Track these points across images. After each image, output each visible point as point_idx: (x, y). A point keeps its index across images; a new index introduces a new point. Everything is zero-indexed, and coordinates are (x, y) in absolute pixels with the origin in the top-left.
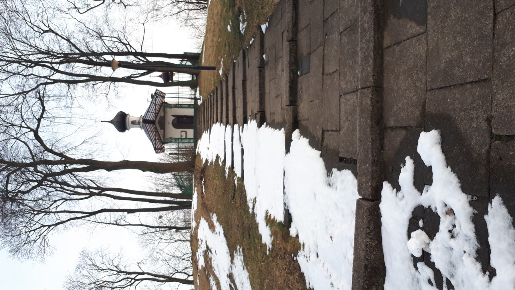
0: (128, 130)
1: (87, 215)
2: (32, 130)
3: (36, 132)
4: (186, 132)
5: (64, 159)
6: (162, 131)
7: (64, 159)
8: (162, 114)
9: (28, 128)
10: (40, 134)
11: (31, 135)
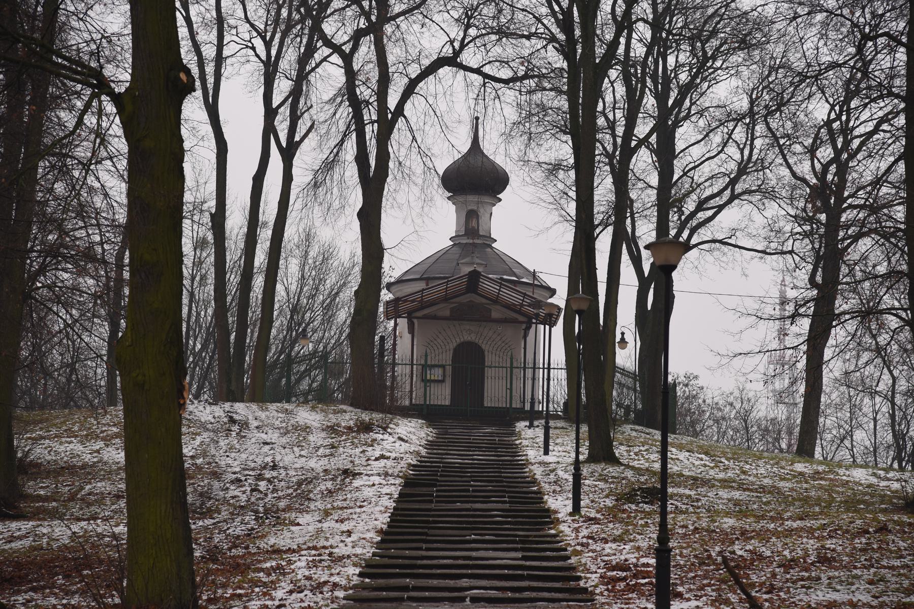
2: (457, 53)
3: (452, 61)
4: (443, 381)
5: (390, 116)
6: (447, 313)
7: (390, 116)
8: (495, 315)
9: (463, 46)
10: (445, 71)
11: (448, 51)
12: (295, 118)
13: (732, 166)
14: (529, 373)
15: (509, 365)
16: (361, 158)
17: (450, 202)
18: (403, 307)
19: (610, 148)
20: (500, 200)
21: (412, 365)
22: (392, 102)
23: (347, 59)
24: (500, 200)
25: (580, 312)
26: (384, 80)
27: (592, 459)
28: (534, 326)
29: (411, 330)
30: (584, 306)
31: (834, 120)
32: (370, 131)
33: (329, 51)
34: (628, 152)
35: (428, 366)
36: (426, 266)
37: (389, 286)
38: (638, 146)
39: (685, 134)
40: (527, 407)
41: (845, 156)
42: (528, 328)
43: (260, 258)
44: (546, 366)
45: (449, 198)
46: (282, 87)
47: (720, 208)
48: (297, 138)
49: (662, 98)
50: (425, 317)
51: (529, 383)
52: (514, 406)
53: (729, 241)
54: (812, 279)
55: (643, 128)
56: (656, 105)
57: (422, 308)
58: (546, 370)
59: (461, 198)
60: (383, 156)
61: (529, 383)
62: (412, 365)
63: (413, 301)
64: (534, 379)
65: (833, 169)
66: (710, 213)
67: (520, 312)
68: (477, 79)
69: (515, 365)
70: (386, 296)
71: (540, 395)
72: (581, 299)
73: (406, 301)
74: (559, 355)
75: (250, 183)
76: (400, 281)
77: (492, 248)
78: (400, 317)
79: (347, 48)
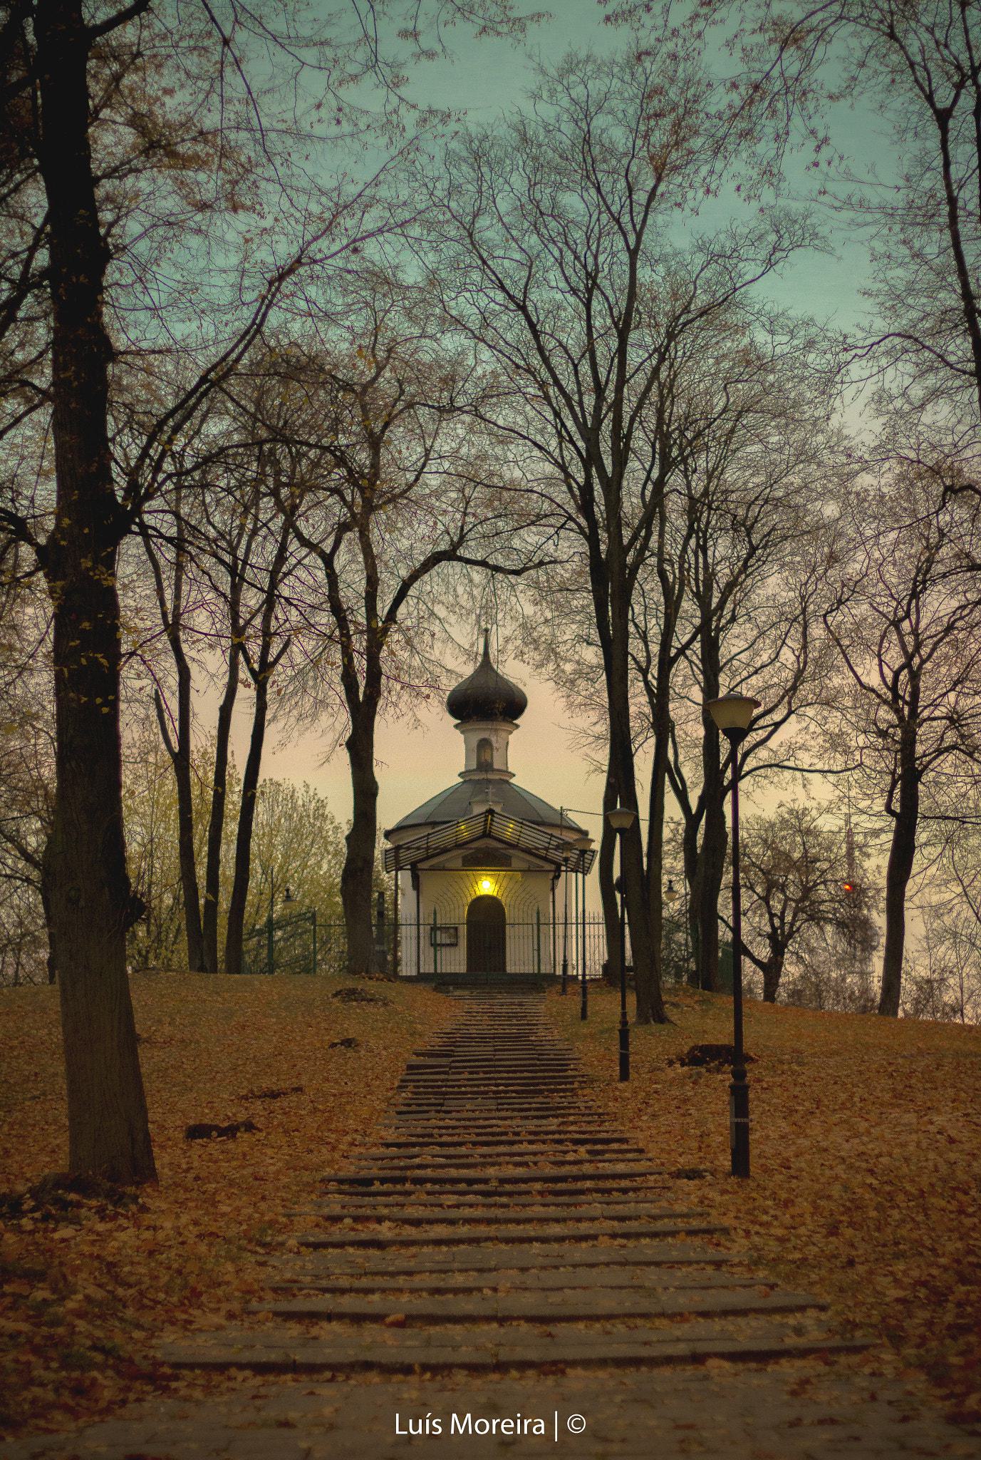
0: (457, 726)
1: (241, 658)
4: (454, 945)
10: (445, 567)
11: (443, 546)
12: (267, 635)
13: (788, 675)
14: (560, 929)
15: (535, 921)
16: (349, 678)
17: (458, 732)
18: (403, 854)
19: (641, 657)
20: (517, 726)
21: (418, 925)
22: (383, 608)
23: (328, 560)
24: (517, 726)
25: (622, 831)
26: (373, 582)
27: (643, 1018)
28: (563, 874)
29: (416, 885)
30: (627, 823)
31: (903, 619)
32: (359, 643)
33: (305, 551)
34: (667, 663)
35: (439, 929)
36: (441, 799)
37: (388, 834)
38: (677, 656)
39: (732, 644)
40: (559, 972)
41: (916, 661)
42: (557, 877)
43: (234, 799)
44: (580, 921)
45: (457, 726)
46: (252, 599)
47: (777, 725)
48: (270, 659)
49: (703, 599)
50: (432, 869)
51: (560, 942)
52: (543, 971)
53: (786, 763)
54: (888, 809)
55: (683, 633)
56: (182, 900)
57: (428, 858)
58: (580, 927)
59: (468, 726)
60: (374, 674)
61: (560, 942)
62: (418, 925)
63: (418, 848)
64: (565, 937)
65: (904, 676)
66: (762, 734)
67: (545, 859)
68: (478, 575)
69: (542, 921)
70: (382, 844)
71: (573, 958)
72: (620, 813)
73: (408, 848)
74: (595, 906)
75: (217, 715)
76: (400, 829)
77: (510, 784)
78: (401, 869)
79: (327, 547)
